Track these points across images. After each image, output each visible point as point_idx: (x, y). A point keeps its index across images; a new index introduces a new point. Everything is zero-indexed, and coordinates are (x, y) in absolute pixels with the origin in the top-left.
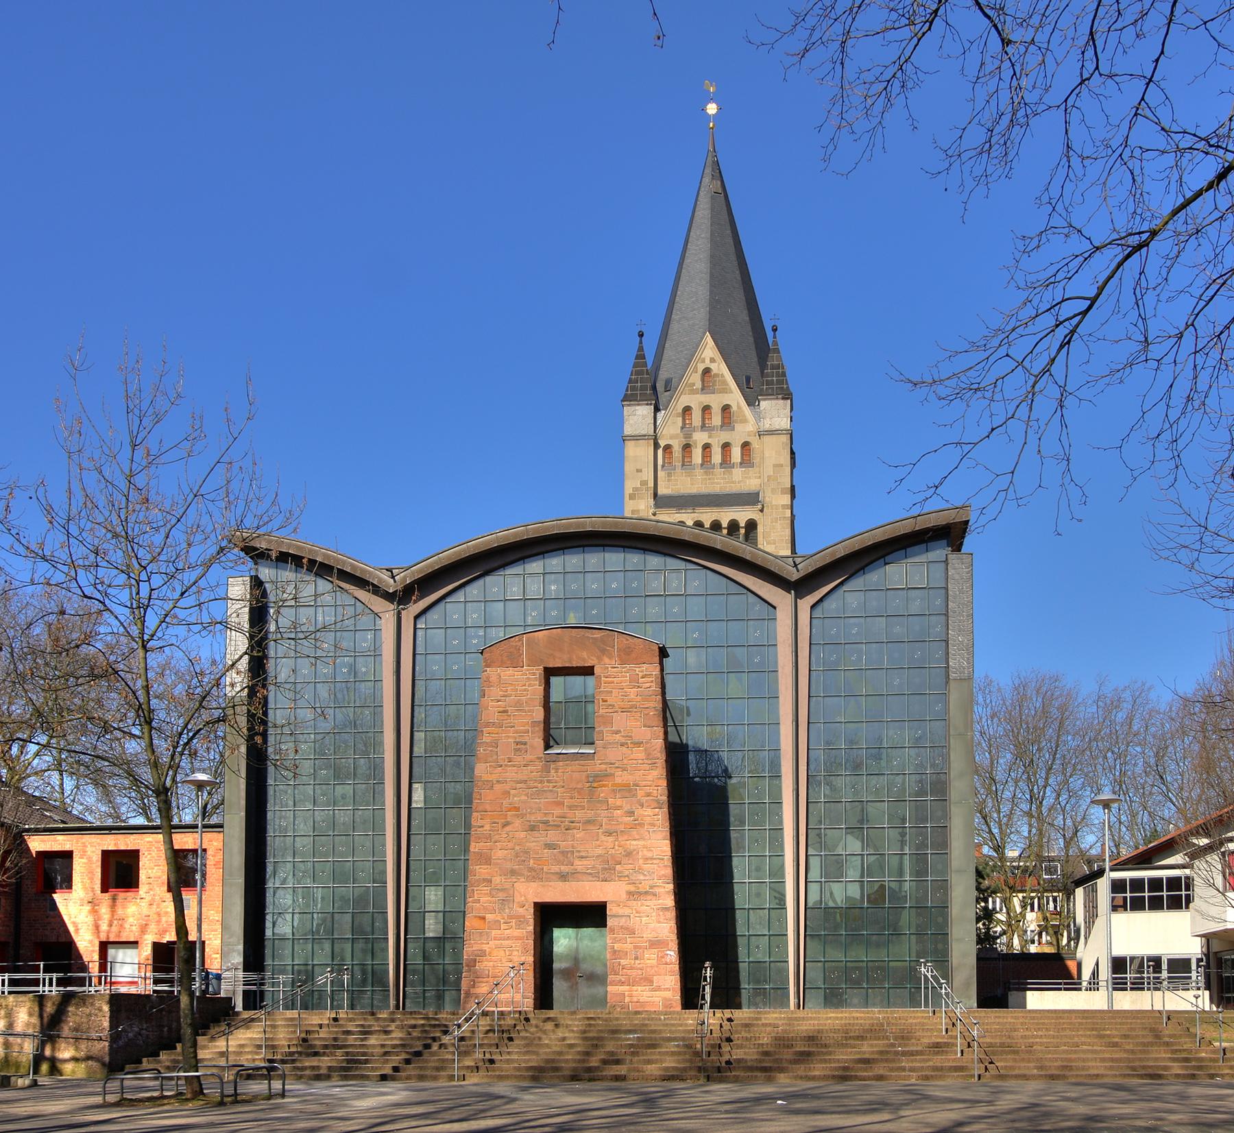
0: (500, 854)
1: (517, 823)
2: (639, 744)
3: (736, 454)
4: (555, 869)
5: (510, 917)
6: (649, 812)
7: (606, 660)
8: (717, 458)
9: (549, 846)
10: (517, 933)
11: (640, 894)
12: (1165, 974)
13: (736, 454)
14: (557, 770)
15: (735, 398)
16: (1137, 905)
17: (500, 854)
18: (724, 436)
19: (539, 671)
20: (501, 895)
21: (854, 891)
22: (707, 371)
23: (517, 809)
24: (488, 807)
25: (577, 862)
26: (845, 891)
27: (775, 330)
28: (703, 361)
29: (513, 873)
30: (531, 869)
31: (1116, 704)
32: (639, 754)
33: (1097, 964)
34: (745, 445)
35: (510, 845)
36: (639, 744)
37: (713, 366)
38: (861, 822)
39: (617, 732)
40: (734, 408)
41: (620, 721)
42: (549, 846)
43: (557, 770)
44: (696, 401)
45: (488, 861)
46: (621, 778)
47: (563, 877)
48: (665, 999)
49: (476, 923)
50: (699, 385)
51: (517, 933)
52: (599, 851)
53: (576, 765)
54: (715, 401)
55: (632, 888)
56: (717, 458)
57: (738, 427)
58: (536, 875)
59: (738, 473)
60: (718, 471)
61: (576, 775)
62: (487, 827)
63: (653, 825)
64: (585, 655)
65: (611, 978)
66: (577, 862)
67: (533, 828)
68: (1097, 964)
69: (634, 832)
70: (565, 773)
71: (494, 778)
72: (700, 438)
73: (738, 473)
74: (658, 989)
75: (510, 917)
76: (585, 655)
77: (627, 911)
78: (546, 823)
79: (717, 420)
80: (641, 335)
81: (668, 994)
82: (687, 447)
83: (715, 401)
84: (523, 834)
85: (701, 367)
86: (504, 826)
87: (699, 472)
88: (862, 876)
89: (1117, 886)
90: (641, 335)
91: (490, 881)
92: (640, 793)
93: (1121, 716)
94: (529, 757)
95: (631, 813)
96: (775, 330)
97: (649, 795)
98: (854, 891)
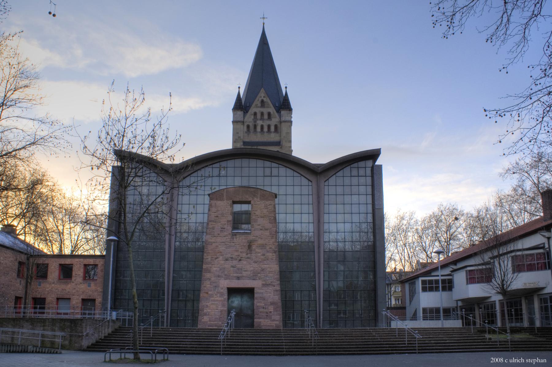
0: (215, 269)
1: (221, 258)
2: (267, 230)
3: (273, 128)
4: (235, 275)
5: (218, 293)
6: (271, 254)
7: (256, 199)
8: (266, 129)
9: (233, 267)
10: (220, 299)
11: (267, 285)
12: (514, 317)
13: (273, 128)
14: (236, 238)
15: (272, 110)
16: (431, 289)
17: (215, 269)
18: (268, 122)
19: (230, 202)
20: (214, 284)
21: (341, 284)
22: (262, 101)
23: (221, 252)
24: (210, 252)
25: (243, 272)
26: (338, 284)
27: (286, 88)
28: (261, 97)
29: (219, 276)
30: (225, 275)
31: (403, 218)
32: (267, 233)
33: (264, 44)
34: (276, 127)
35: (218, 266)
36: (267, 230)
37: (265, 99)
38: (329, 259)
39: (259, 225)
40: (272, 113)
41: (260, 221)
42: (233, 267)
43: (236, 238)
44: (258, 110)
45: (210, 272)
46: (260, 242)
47: (238, 278)
48: (276, 324)
49: (206, 295)
50: (259, 105)
51: (220, 299)
52: (252, 269)
53: (243, 237)
54: (265, 111)
55: (264, 283)
56: (266, 129)
57: (273, 119)
58: (227, 277)
59: (273, 135)
60: (266, 134)
61: (243, 240)
62: (210, 259)
63: (272, 259)
64: (247, 197)
65: (256, 316)
66: (243, 272)
67: (227, 260)
68: (264, 44)
69: (265, 262)
70: (241, 240)
71: (213, 240)
72: (259, 123)
73: (273, 135)
74: (274, 320)
75: (218, 293)
76: (247, 197)
77: (262, 291)
78: (232, 258)
79: (266, 117)
80: (239, 88)
81: (277, 322)
82: (255, 127)
83: (265, 111)
84: (223, 262)
85: (260, 99)
86: (216, 258)
87: (259, 135)
88: (344, 278)
89: (424, 282)
90: (239, 88)
91: (210, 279)
92: (268, 248)
93: (405, 222)
94: (225, 233)
95: (264, 255)
96: (286, 88)
97: (271, 248)
98: (341, 284)
